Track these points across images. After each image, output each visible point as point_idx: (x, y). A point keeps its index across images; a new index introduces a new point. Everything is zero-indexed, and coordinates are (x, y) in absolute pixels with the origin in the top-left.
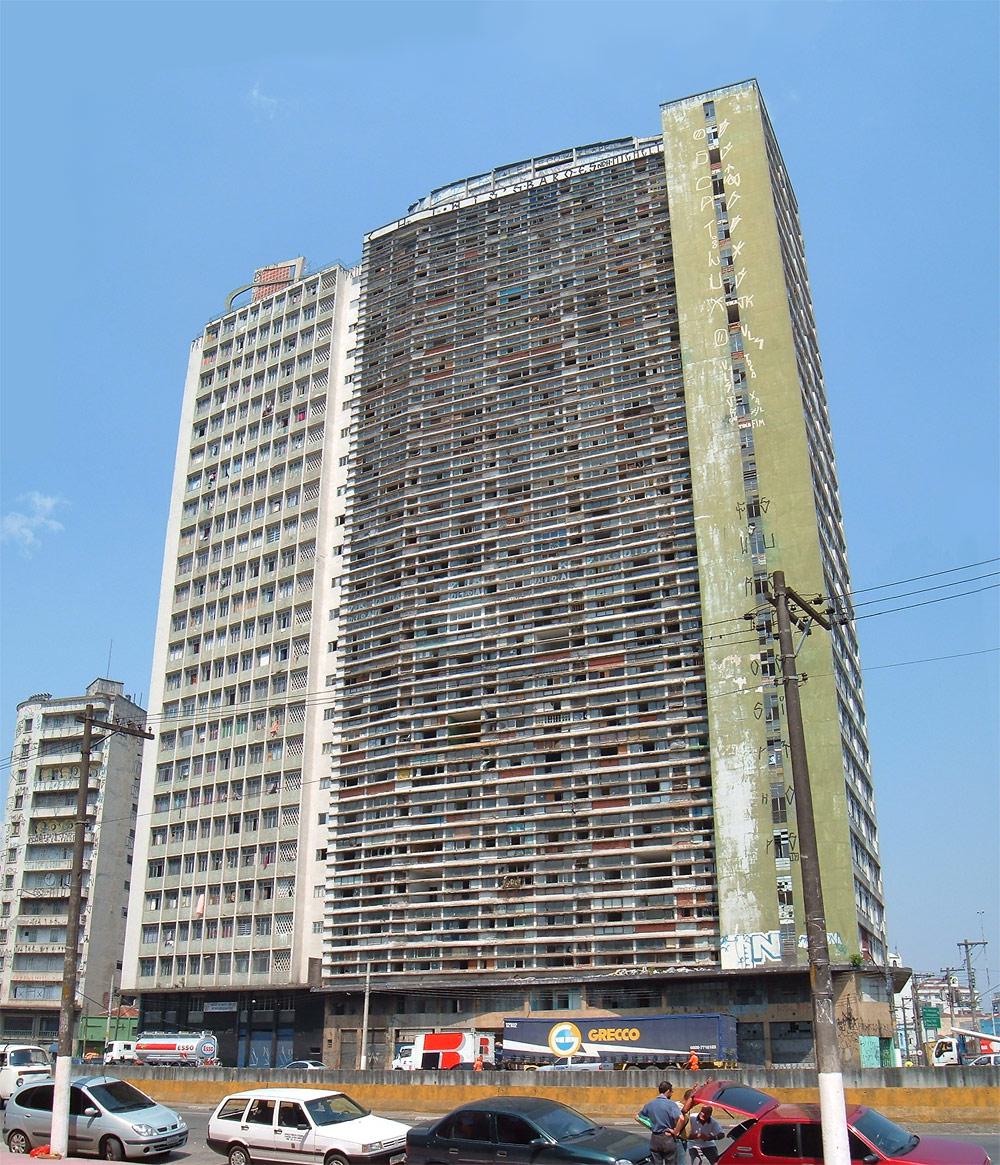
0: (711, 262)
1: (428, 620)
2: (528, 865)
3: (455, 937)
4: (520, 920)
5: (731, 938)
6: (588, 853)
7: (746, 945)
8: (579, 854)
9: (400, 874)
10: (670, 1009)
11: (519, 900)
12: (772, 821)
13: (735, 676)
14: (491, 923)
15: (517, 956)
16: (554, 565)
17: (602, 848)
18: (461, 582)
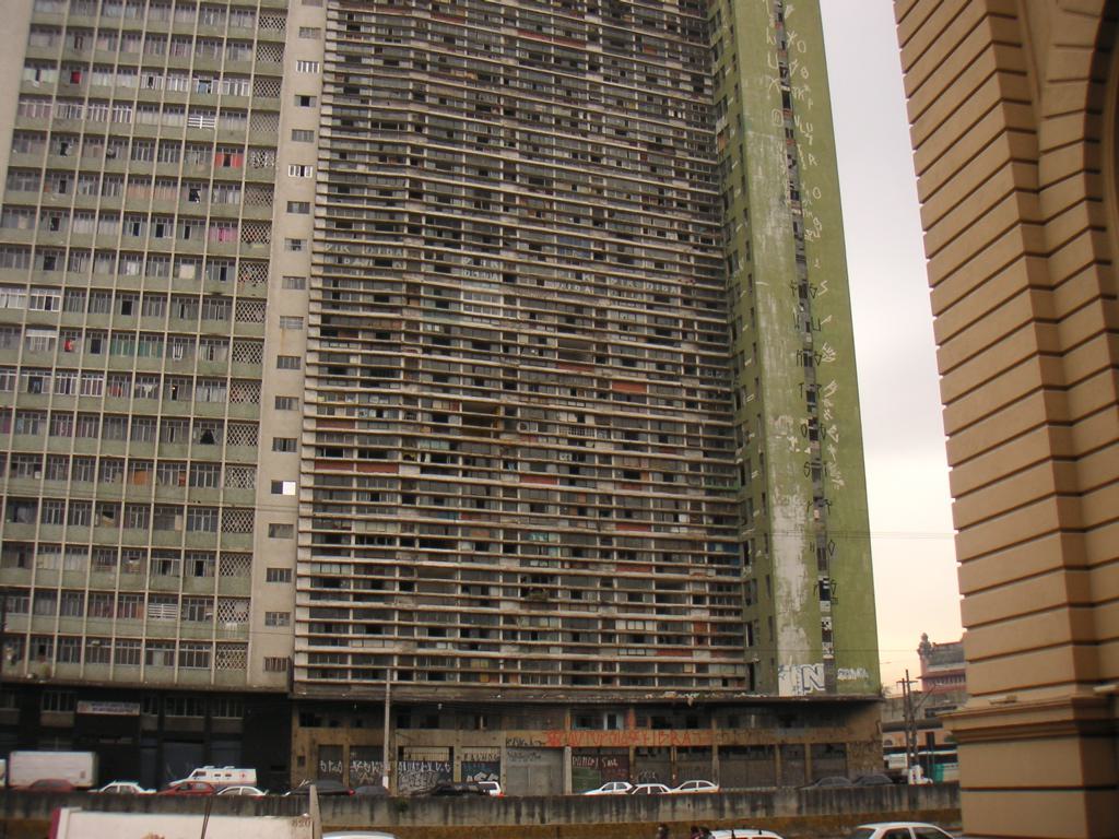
0: (769, 39)
1: (438, 290)
2: (552, 577)
3: (473, 646)
4: (545, 633)
5: (786, 668)
6: (612, 571)
7: (796, 680)
8: (603, 572)
9: (405, 569)
10: (720, 731)
11: (542, 613)
12: (816, 567)
13: (789, 434)
14: (513, 634)
15: (536, 669)
16: (579, 274)
17: (626, 570)
18: (477, 260)
